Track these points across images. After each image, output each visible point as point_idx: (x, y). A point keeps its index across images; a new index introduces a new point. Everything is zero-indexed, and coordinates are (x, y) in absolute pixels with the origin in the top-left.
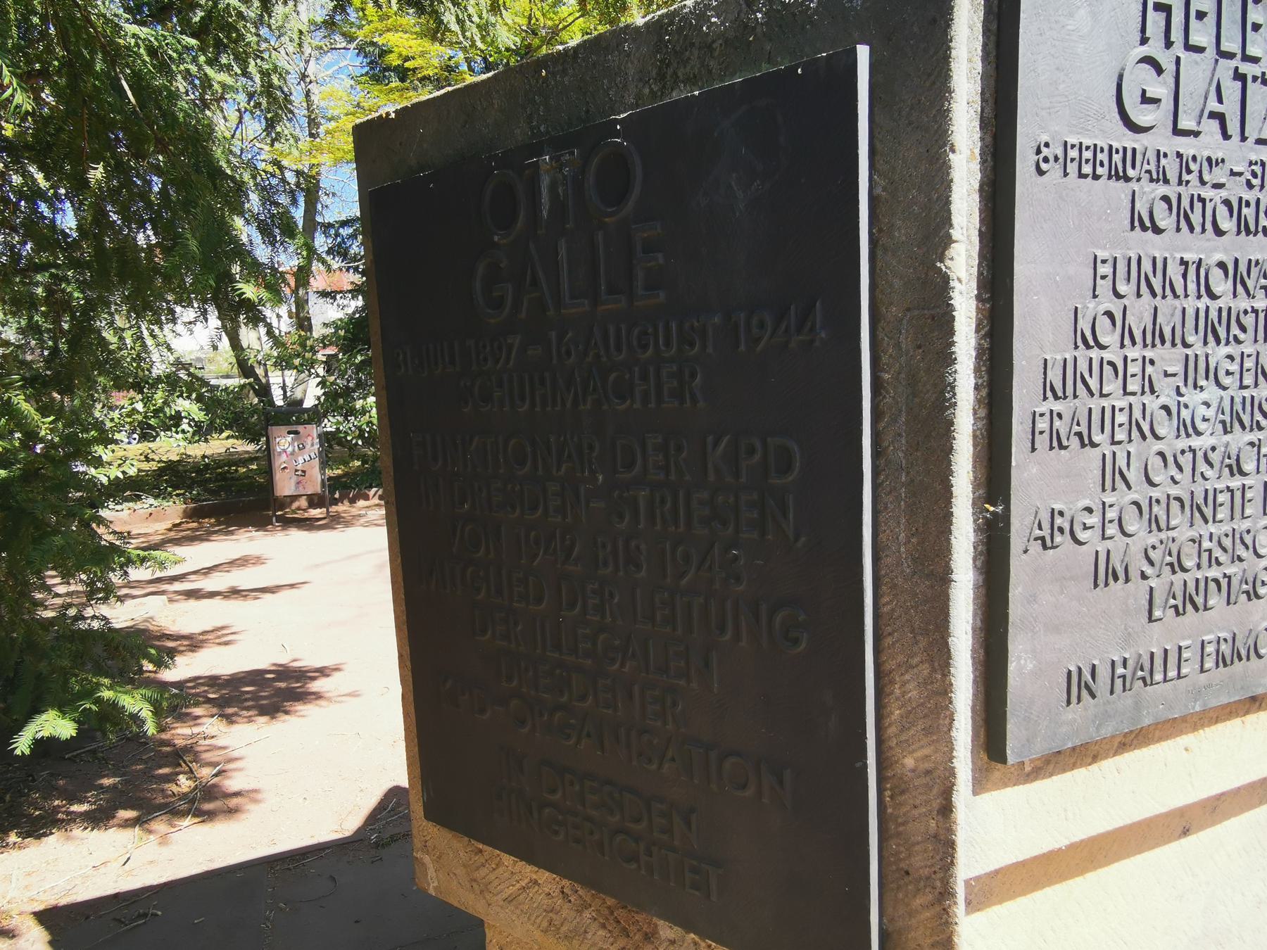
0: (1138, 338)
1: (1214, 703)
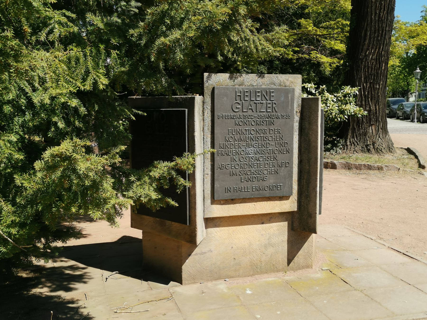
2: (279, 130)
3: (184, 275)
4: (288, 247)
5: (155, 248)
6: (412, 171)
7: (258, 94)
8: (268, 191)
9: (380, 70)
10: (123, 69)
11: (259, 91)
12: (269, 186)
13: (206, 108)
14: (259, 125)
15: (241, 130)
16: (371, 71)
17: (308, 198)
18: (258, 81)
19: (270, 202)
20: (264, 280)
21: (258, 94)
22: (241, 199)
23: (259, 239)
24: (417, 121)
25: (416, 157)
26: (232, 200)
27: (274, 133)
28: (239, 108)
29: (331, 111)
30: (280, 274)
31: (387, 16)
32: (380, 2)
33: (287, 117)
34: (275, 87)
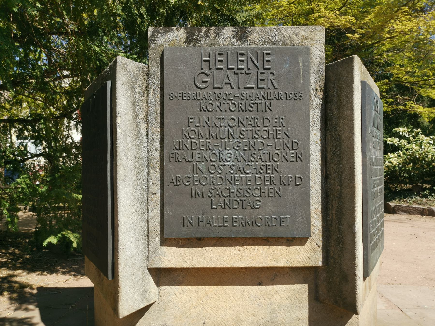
2: (281, 120)
8: (263, 227)
12: (263, 219)
13: (151, 84)
15: (210, 119)
17: (339, 243)
19: (268, 247)
23: (253, 312)
26: (199, 239)
27: (271, 126)
29: (427, 153)
33: (296, 97)
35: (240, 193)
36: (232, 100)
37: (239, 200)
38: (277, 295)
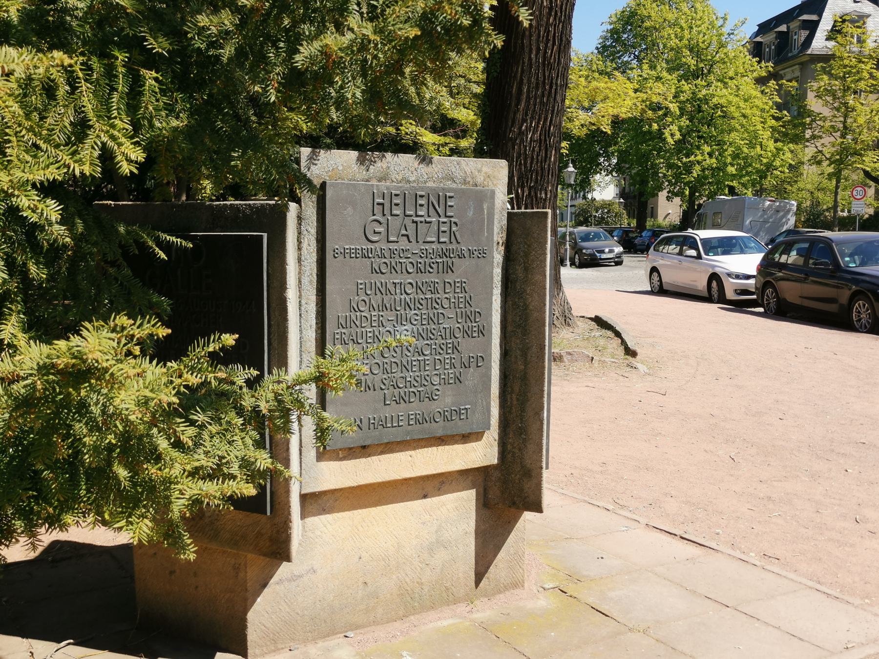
0: (376, 308)
1: (416, 437)
2: (464, 285)
3: (253, 635)
4: (476, 546)
5: (172, 573)
6: (616, 363)
7: (420, 202)
9: (547, 163)
10: (175, 123)
11: (423, 193)
13: (305, 232)
14: (422, 272)
16: (531, 163)
17: (521, 434)
18: (419, 170)
19: (443, 447)
20: (431, 625)
21: (420, 202)
22: (382, 444)
23: (417, 534)
24: (571, 265)
25: (618, 334)
26: (364, 447)
28: (380, 233)
30: (462, 608)
31: (559, 56)
32: (546, 28)
33: (480, 254)
34: (454, 186)
35: (417, 381)
36: (409, 258)
37: (416, 391)
38: (444, 507)
